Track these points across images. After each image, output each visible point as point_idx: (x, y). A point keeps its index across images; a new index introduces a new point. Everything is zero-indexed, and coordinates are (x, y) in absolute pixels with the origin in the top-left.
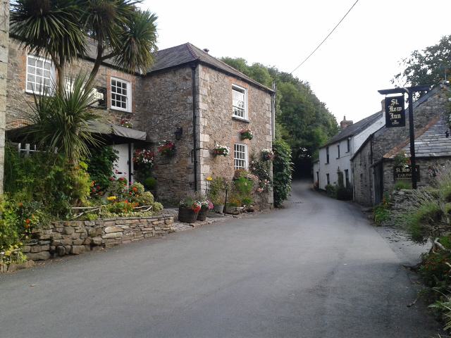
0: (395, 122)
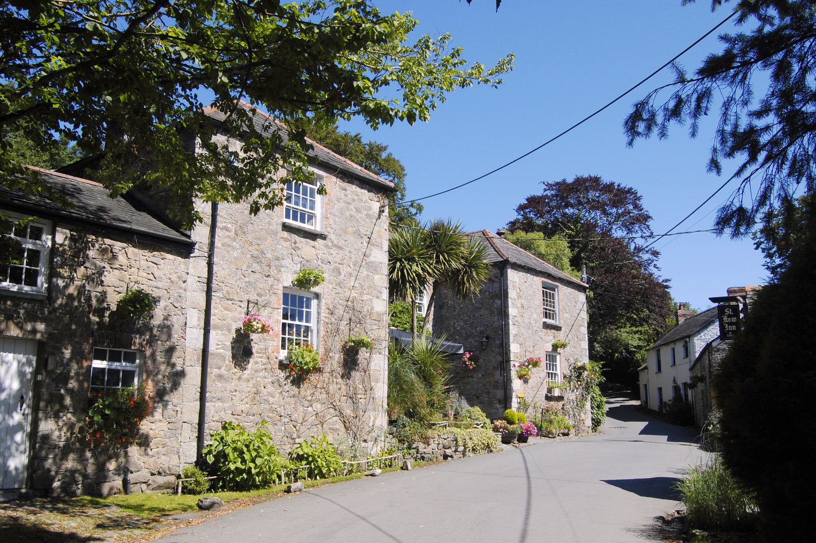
0: (730, 335)
